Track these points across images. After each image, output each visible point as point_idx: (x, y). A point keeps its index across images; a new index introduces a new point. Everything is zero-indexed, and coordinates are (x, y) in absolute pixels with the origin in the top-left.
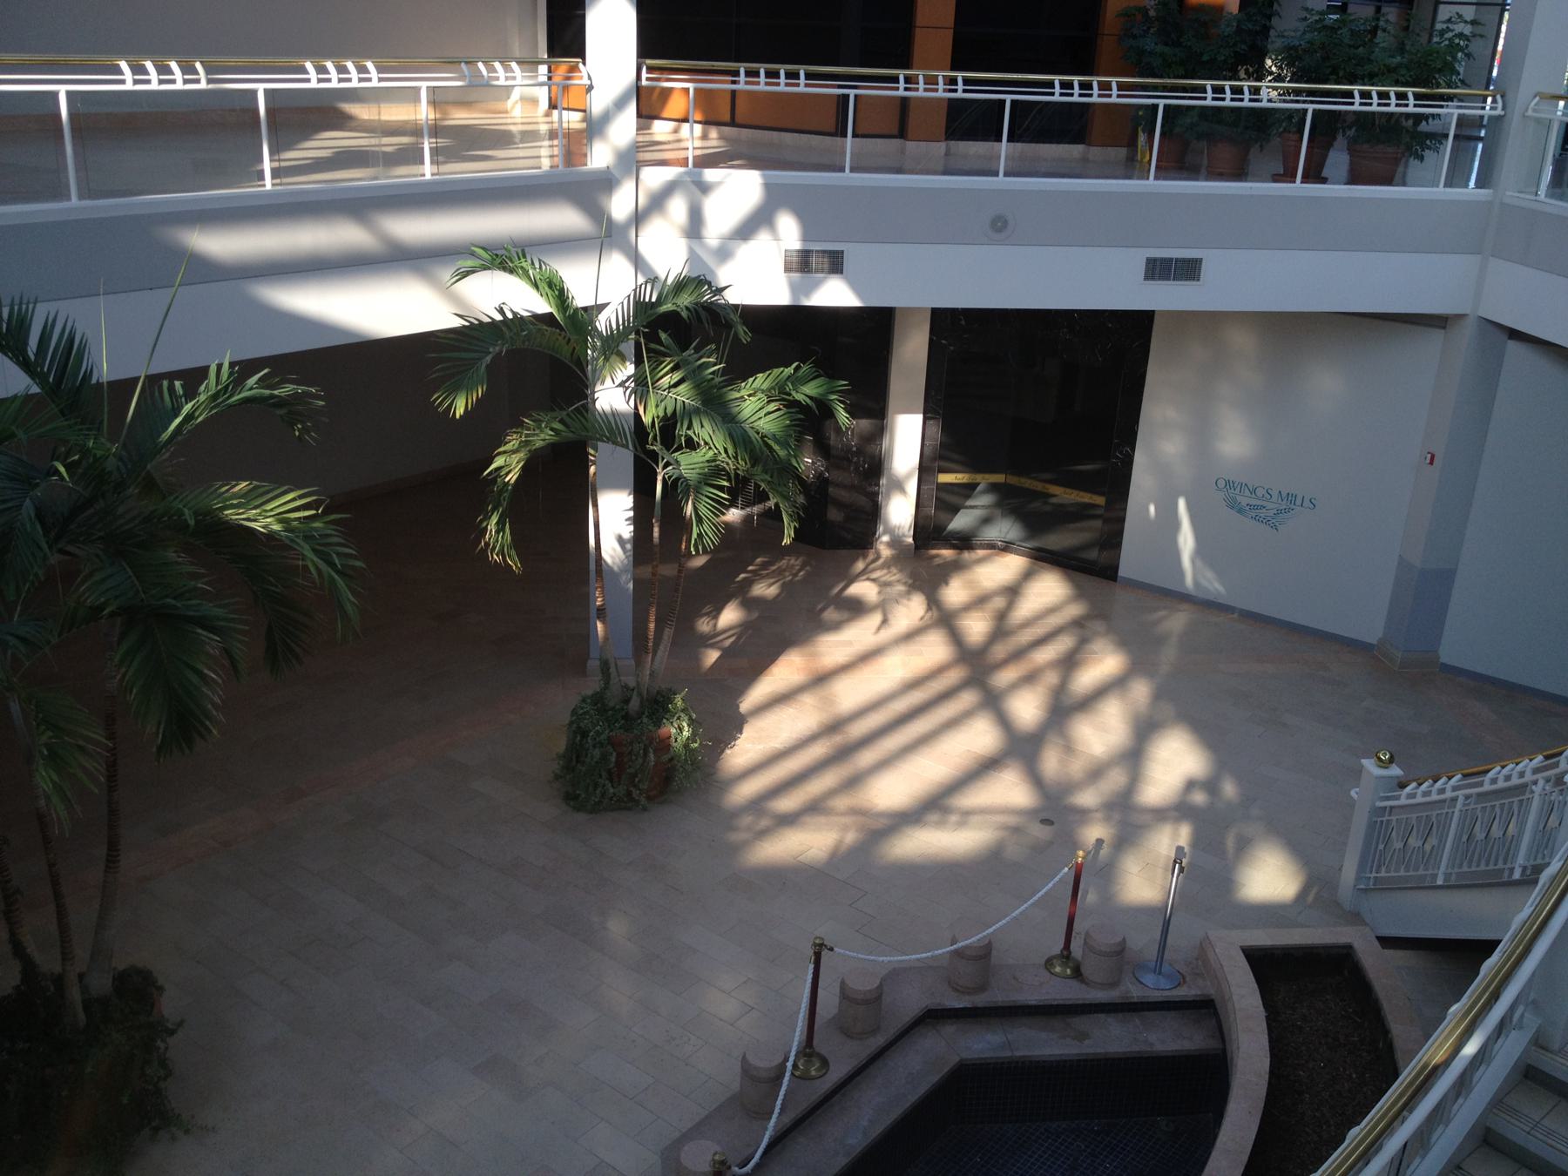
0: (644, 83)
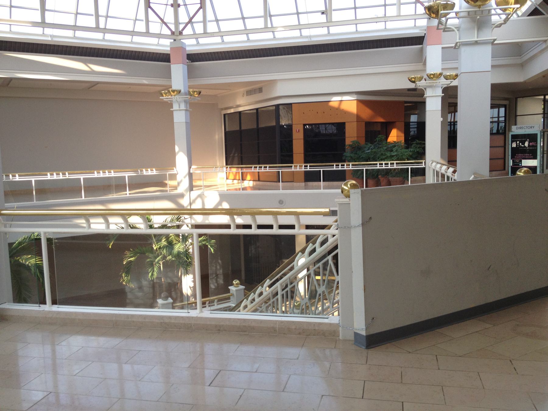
0: (191, 172)
